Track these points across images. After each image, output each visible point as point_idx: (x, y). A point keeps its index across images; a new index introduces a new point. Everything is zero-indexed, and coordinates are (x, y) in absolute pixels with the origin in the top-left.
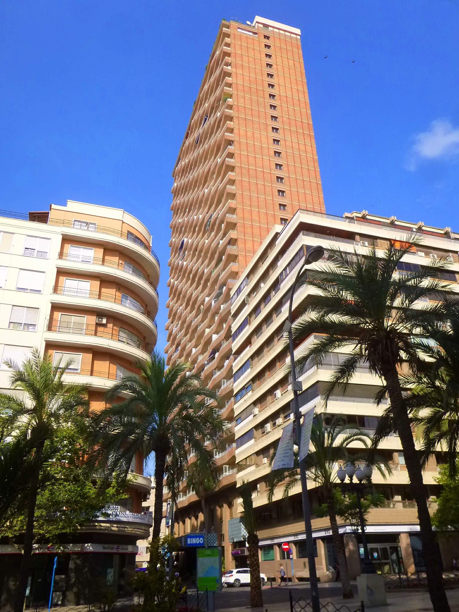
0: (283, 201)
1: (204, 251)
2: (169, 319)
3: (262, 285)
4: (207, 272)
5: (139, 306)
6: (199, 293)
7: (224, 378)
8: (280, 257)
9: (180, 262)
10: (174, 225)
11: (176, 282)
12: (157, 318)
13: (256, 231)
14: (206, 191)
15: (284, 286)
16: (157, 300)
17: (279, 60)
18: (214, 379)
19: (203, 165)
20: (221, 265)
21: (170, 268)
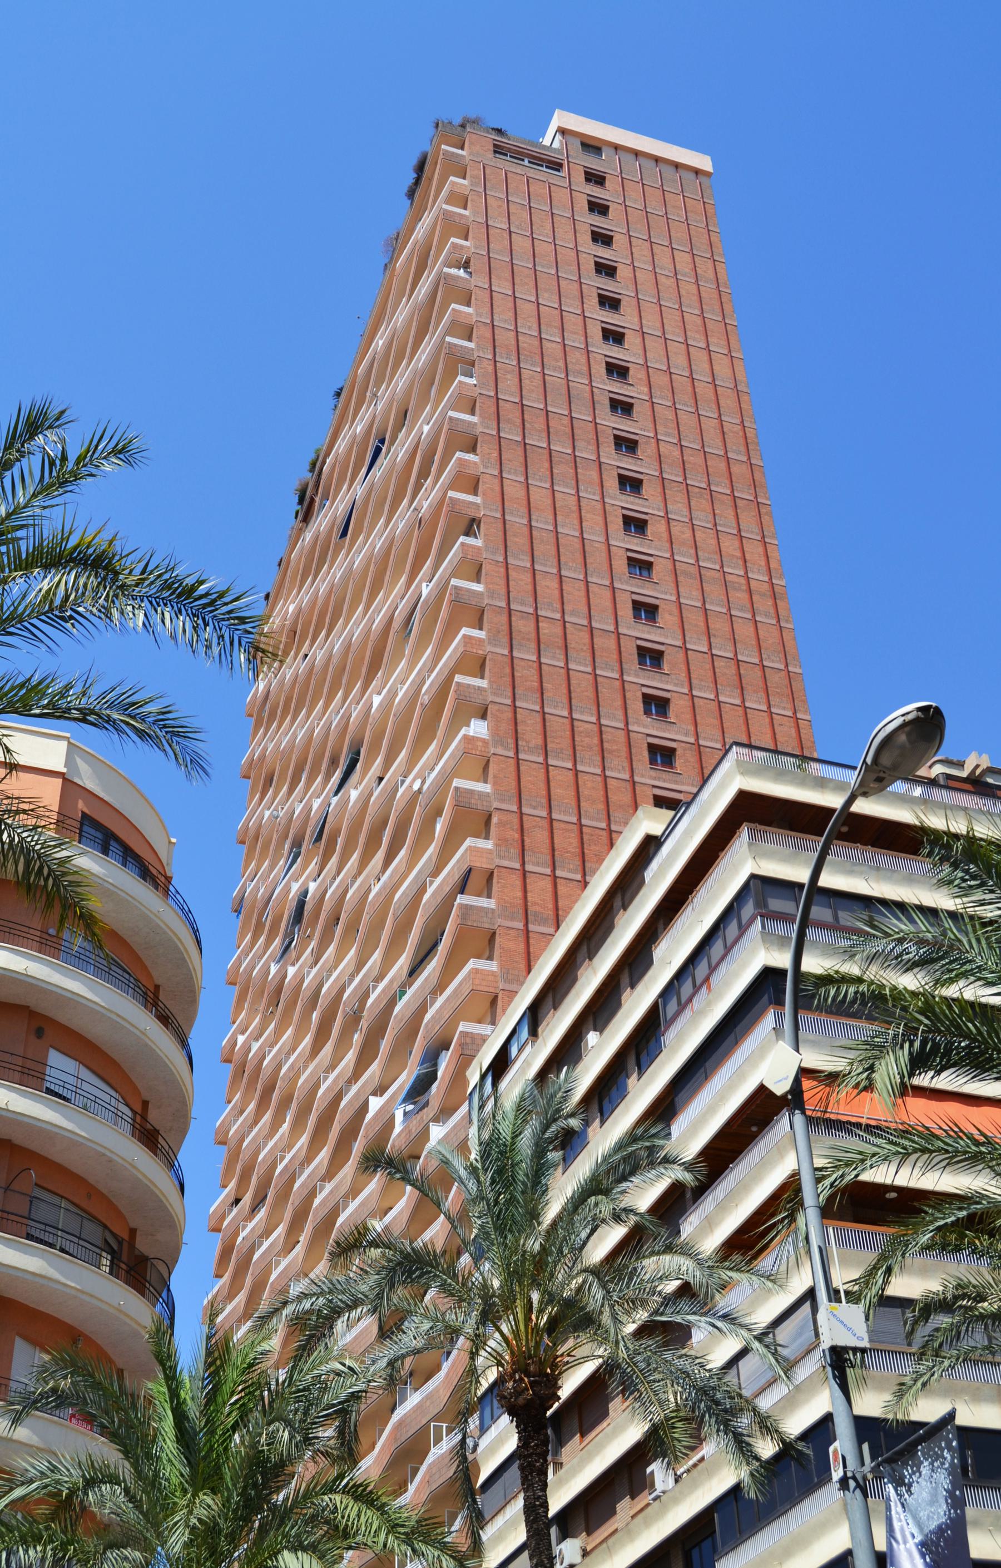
0: (647, 592)
1: (364, 1024)
2: (219, 1276)
3: (592, 1038)
4: (381, 704)
5: (113, 1102)
6: (341, 1083)
7: (436, 1418)
8: (661, 926)
9: (274, 969)
10: (251, 833)
11: (255, 1047)
12: (185, 1157)
13: (567, 842)
14: (377, 700)
15: (681, 1038)
16: (189, 1087)
17: (642, 251)
18: (401, 1423)
19: (366, 611)
20: (433, 967)
21: (236, 990)
